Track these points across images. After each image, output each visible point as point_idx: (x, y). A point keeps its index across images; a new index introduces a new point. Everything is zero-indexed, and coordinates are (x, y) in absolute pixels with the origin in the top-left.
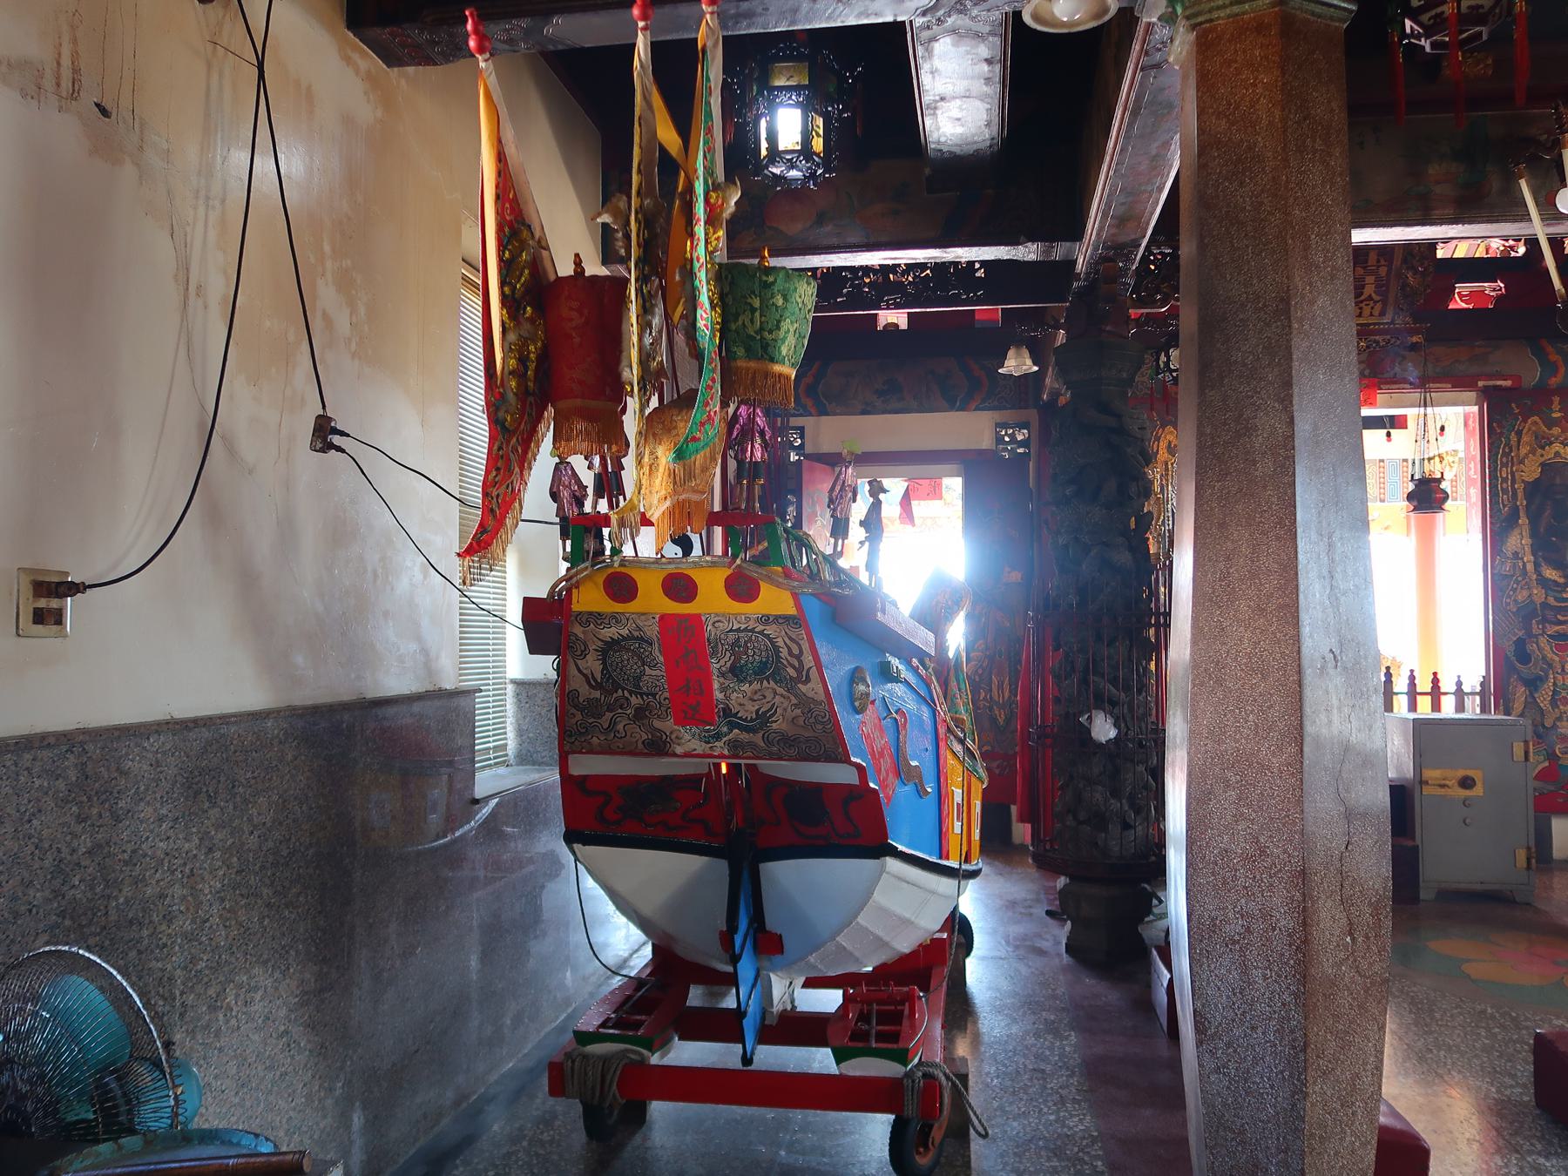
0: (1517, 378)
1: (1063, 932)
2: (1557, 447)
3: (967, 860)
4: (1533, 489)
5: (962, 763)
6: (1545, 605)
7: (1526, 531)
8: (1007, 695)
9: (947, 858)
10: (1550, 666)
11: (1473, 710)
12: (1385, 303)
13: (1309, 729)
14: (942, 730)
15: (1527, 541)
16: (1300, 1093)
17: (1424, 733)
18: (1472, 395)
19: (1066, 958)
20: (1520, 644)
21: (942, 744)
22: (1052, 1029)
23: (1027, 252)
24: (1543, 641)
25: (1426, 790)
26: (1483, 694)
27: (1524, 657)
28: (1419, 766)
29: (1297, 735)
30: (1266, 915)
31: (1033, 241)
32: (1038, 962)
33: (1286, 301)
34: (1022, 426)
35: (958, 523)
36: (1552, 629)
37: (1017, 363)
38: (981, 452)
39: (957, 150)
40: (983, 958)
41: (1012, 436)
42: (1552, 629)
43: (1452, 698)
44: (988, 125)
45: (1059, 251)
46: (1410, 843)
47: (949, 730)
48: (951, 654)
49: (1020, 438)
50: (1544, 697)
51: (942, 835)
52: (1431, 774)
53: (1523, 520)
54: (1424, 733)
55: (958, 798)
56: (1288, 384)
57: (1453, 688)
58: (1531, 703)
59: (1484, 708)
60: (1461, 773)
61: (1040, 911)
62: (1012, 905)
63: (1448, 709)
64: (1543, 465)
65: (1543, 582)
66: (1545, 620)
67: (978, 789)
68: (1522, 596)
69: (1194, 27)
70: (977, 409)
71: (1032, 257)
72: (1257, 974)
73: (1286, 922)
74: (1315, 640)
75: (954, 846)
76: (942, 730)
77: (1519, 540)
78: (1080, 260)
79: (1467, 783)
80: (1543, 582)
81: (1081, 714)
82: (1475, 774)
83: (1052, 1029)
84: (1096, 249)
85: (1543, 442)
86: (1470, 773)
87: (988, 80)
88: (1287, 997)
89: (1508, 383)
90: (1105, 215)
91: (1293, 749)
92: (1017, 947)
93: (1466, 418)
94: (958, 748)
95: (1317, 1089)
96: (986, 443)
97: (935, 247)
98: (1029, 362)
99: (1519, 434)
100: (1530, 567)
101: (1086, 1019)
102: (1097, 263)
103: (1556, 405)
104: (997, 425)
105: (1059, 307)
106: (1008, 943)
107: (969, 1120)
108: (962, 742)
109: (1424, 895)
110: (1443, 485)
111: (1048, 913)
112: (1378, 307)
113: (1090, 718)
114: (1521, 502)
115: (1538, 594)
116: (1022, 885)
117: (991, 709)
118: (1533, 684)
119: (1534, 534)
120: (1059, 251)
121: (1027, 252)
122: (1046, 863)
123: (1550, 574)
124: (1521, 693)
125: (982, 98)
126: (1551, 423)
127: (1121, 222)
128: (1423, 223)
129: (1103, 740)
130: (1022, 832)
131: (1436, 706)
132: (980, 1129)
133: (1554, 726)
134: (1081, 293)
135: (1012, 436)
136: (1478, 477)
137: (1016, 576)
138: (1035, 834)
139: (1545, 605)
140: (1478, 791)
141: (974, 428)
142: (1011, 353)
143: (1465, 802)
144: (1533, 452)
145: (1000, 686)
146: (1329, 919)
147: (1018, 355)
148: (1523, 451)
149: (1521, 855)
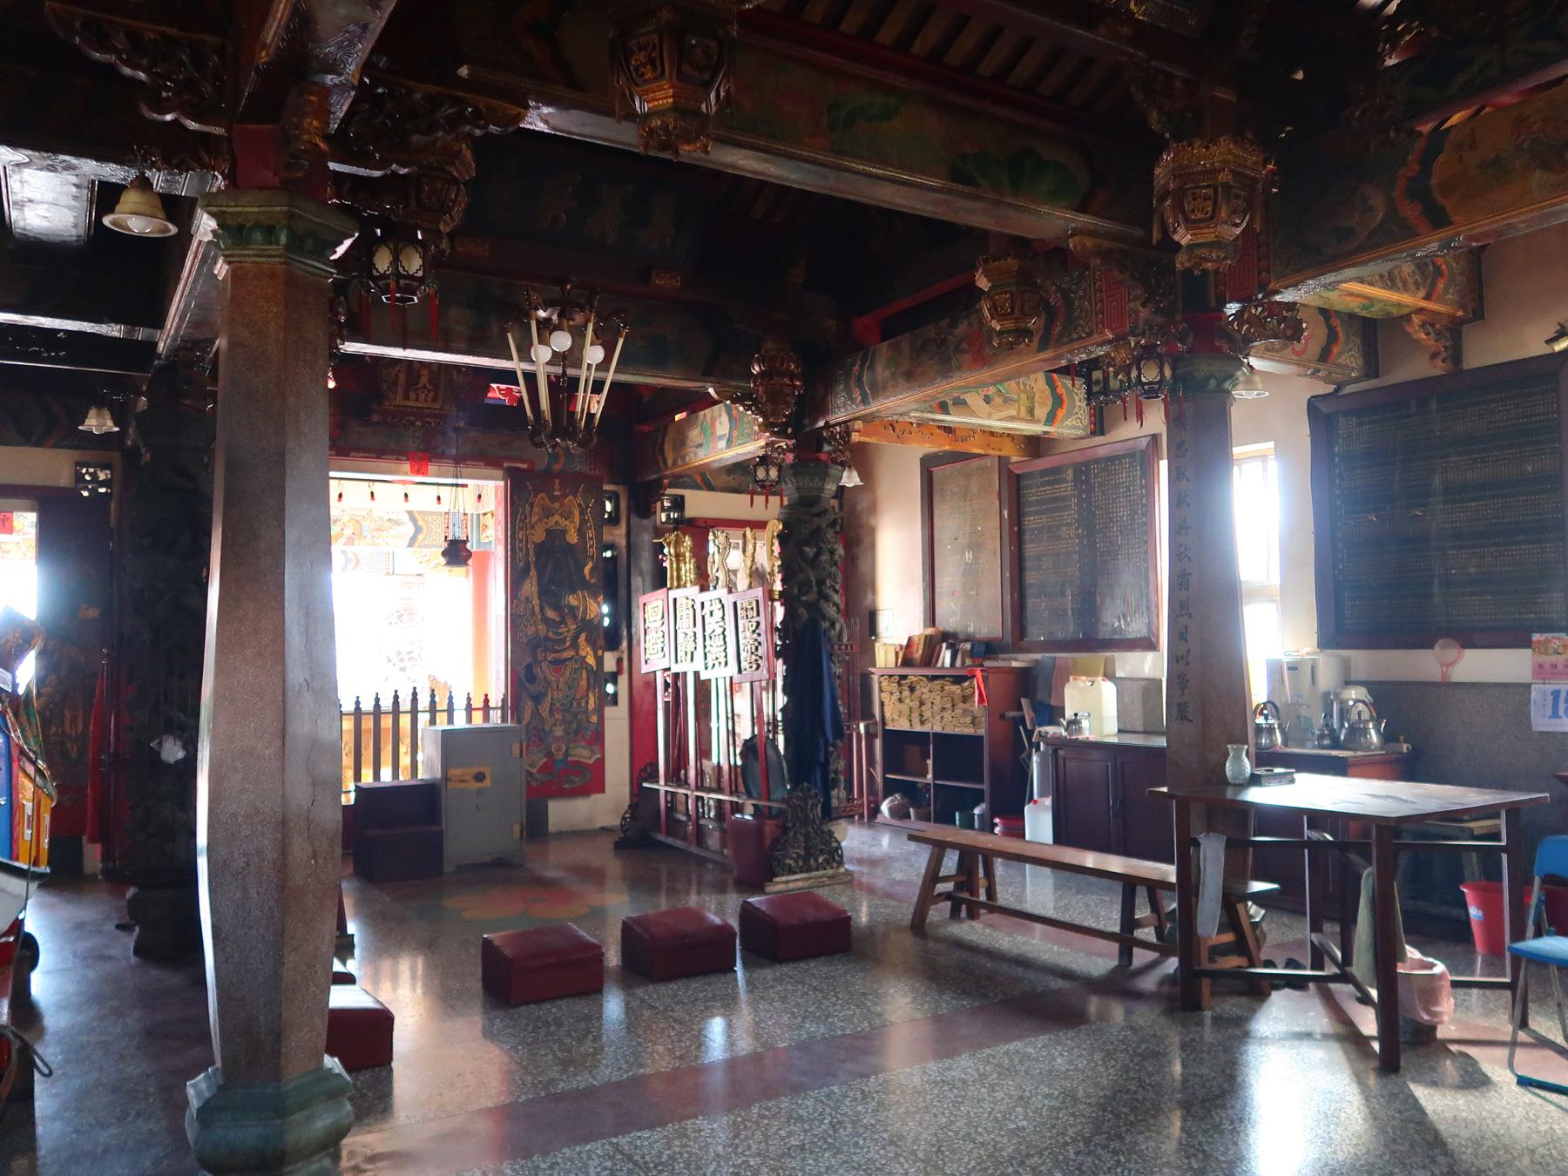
0: (532, 463)
1: (129, 941)
2: (557, 518)
3: (36, 863)
4: (541, 549)
5: (33, 781)
6: (546, 637)
7: (535, 583)
8: (80, 728)
9: (17, 859)
10: (549, 684)
11: (496, 718)
12: (436, 391)
13: (291, 730)
14: (15, 753)
15: (535, 589)
16: (279, 962)
17: (450, 741)
18: (500, 473)
19: (133, 960)
20: (529, 668)
21: (15, 765)
22: (118, 1013)
23: (114, 330)
24: (544, 665)
25: (450, 785)
26: (503, 708)
27: (531, 678)
28: (445, 769)
29: (283, 733)
30: (259, 852)
31: (117, 323)
32: (108, 967)
33: (282, 455)
34: (103, 467)
35: (32, 551)
36: (551, 657)
37: (97, 423)
38: (58, 490)
39: (44, 238)
40: (48, 972)
41: (94, 475)
42: (551, 657)
43: (420, 707)
44: (75, 226)
45: (141, 334)
46: (436, 828)
47: (22, 752)
48: (21, 691)
49: (102, 476)
50: (544, 708)
51: (13, 839)
52: (453, 772)
53: (533, 573)
54: (450, 741)
55: (29, 808)
56: (282, 509)
57: (481, 705)
58: (536, 713)
59: (504, 719)
60: (476, 770)
61: (110, 927)
62: (80, 926)
63: (460, 722)
64: (548, 531)
65: (546, 620)
66: (546, 650)
67: (48, 806)
68: (531, 631)
69: (229, 263)
70: (56, 446)
71: (116, 334)
72: (253, 893)
73: (271, 854)
74: (296, 674)
75: (23, 849)
76: (15, 753)
77: (530, 587)
78: (161, 345)
79: (480, 777)
80: (546, 620)
81: (152, 739)
82: (486, 770)
83: (118, 1013)
84: (174, 340)
85: (548, 513)
86: (482, 769)
87: (75, 198)
88: (272, 903)
89: (524, 466)
90: (182, 319)
91: (278, 743)
92: (85, 958)
93: (497, 488)
94: (31, 770)
95: (291, 959)
96: (65, 480)
97: (16, 312)
98: (110, 423)
99: (532, 505)
100: (537, 609)
101: (149, 998)
102: (175, 351)
103: (557, 486)
104: (77, 464)
105: (143, 378)
106: (75, 956)
107: (34, 1065)
108: (34, 763)
109: (448, 868)
110: (468, 546)
111: (118, 927)
112: (431, 395)
113: (160, 744)
114: (532, 558)
115: (542, 629)
116: (93, 910)
117: (63, 743)
118: (537, 699)
119: (540, 584)
120: (141, 334)
121: (114, 330)
122: (115, 878)
123: (550, 614)
124: (528, 707)
125: (69, 208)
126: (553, 499)
127: (195, 325)
128: (446, 351)
129: (172, 760)
130: (92, 857)
131: (486, 718)
132: (46, 1071)
133: (551, 731)
134: (161, 369)
135: (94, 475)
136: (502, 537)
137: (93, 613)
138: (106, 857)
139: (546, 637)
140: (487, 783)
141: (51, 466)
142: (93, 412)
143: (479, 792)
144: (540, 520)
145: (74, 721)
146: (300, 850)
147: (99, 415)
148: (534, 519)
149: (517, 828)
